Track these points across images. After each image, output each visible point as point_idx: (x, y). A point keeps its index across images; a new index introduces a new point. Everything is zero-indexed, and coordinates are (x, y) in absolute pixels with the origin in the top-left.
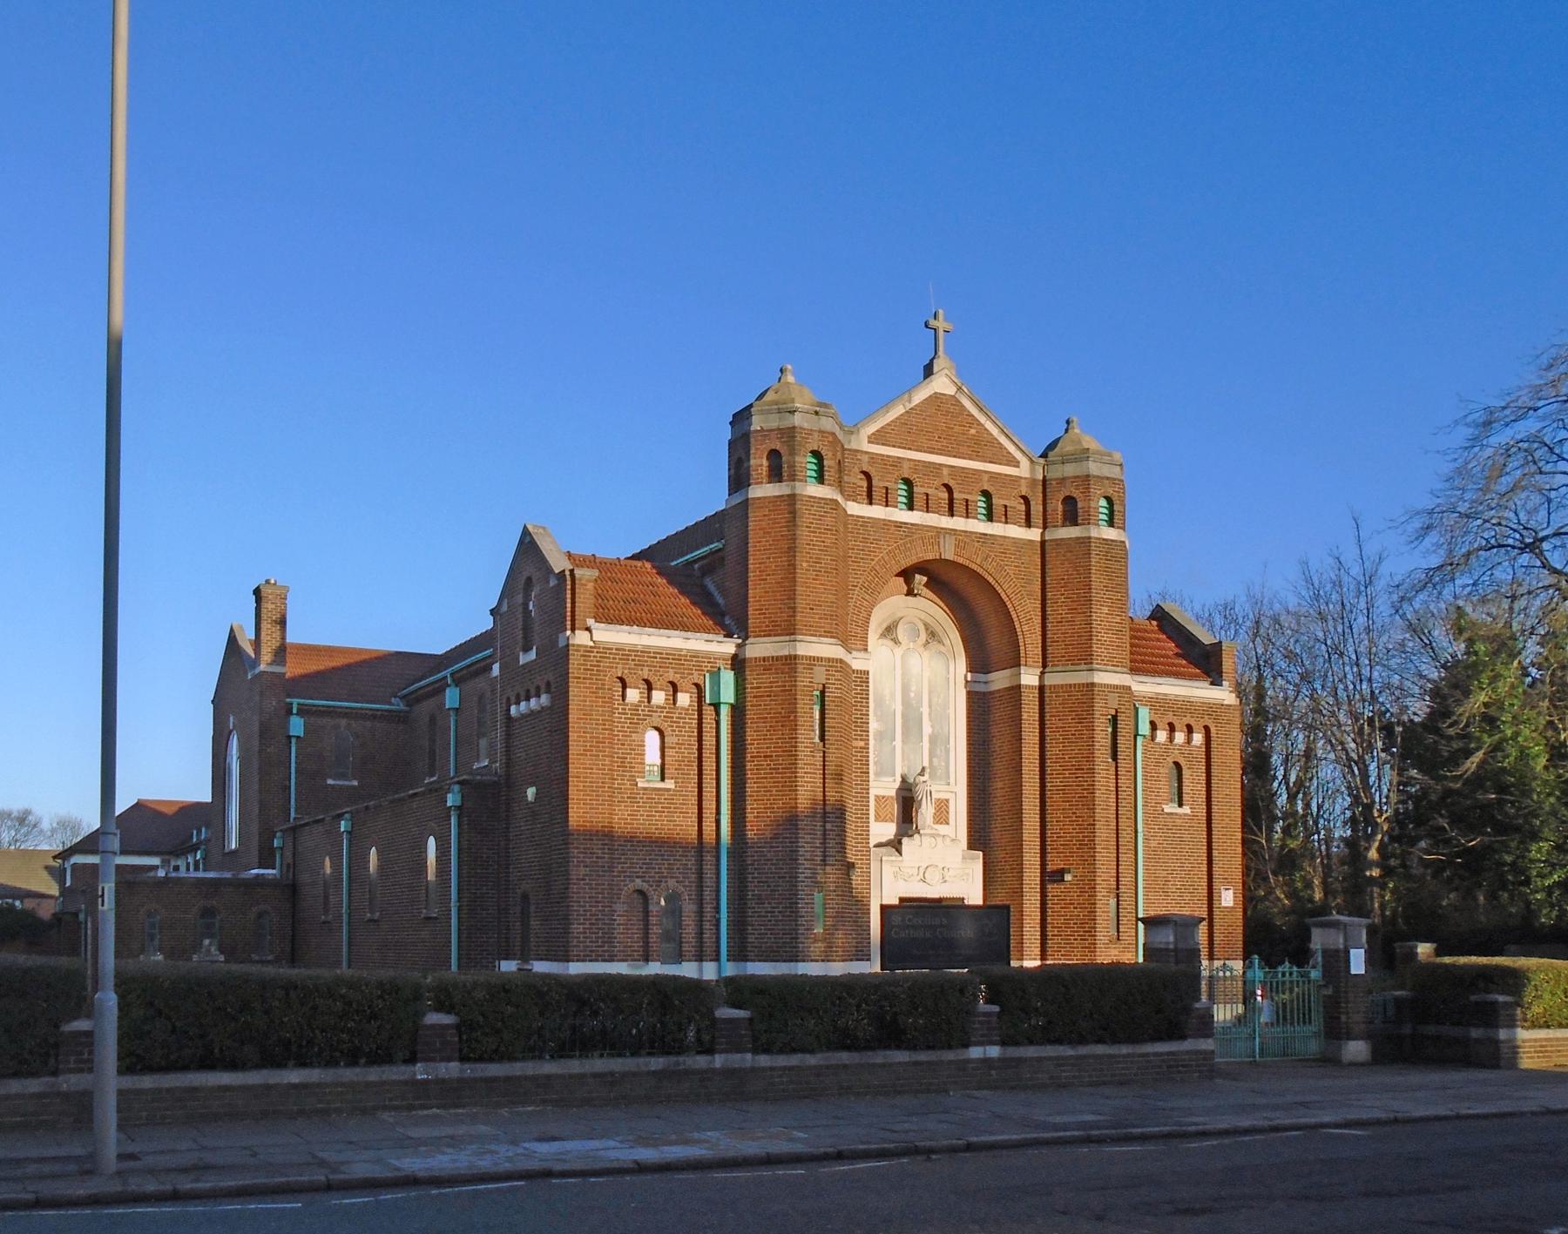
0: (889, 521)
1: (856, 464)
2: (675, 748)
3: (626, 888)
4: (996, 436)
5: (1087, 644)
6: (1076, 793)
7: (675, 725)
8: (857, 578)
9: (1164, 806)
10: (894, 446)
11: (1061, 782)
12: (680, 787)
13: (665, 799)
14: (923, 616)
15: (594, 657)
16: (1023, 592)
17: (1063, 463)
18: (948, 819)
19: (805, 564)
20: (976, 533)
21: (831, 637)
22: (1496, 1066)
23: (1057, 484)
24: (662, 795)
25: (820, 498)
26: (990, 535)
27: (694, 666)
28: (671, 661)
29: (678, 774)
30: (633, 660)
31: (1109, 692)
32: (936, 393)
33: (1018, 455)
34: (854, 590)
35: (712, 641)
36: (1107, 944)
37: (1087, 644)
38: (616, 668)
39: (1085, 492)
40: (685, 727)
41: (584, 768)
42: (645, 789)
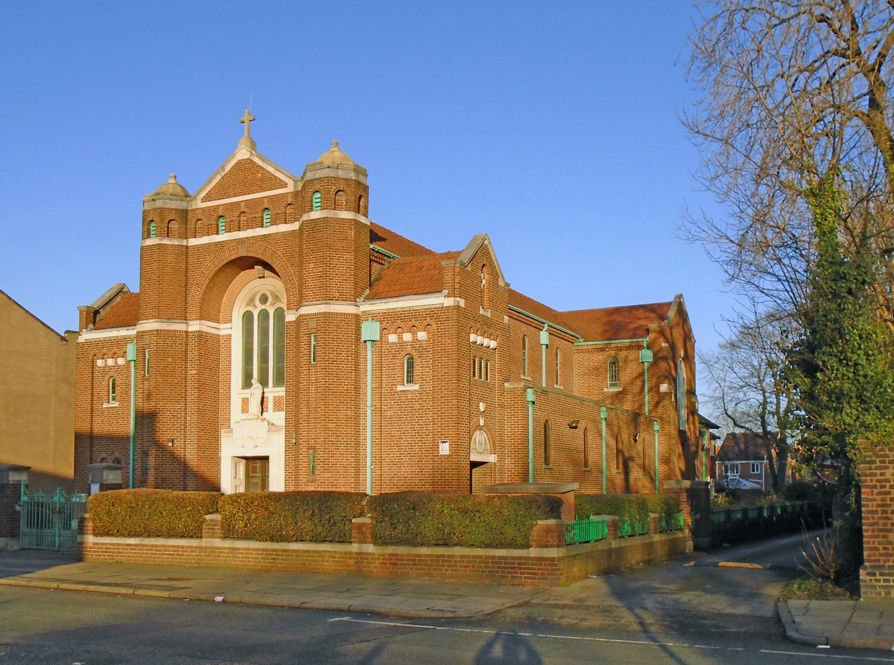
4: (273, 173)
10: (215, 200)
14: (270, 288)
26: (268, 235)
31: (310, 319)
32: (239, 161)
42: (107, 408)
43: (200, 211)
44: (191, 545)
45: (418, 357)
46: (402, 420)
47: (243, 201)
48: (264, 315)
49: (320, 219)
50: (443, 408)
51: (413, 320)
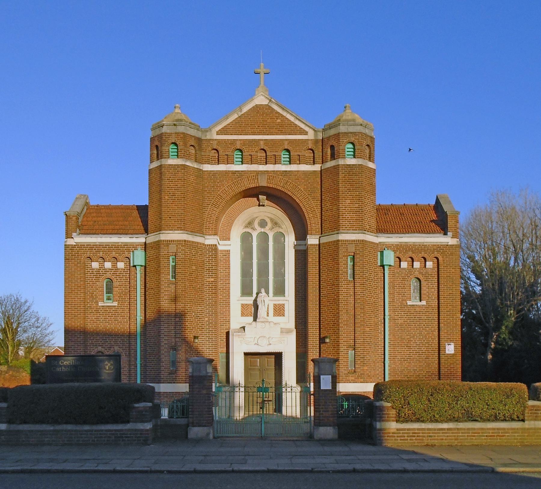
0: (228, 171)
1: (209, 146)
2: (118, 287)
3: (93, 351)
5: (337, 220)
6: (332, 297)
7: (118, 277)
8: (210, 201)
9: (408, 302)
11: (326, 292)
12: (120, 305)
13: (113, 311)
14: (270, 215)
15: (76, 249)
16: (309, 197)
17: (330, 129)
18: (284, 313)
19: (166, 197)
20: (280, 171)
21: (181, 230)
22: (374, 444)
23: (327, 140)
24: (111, 309)
25: (175, 165)
26: (289, 171)
27: (125, 249)
28: (114, 248)
29: (120, 299)
30: (95, 249)
31: (348, 244)
32: (256, 105)
33: (307, 129)
34: (208, 207)
35: (133, 237)
36: (348, 374)
37: (337, 220)
38: (87, 253)
39: (337, 142)
40: (123, 278)
41: (71, 299)
43: (216, 142)
44: (513, 427)
45: (425, 281)
46: (411, 327)
47: (262, 140)
48: (264, 237)
49: (356, 165)
50: (449, 319)
51: (423, 252)
